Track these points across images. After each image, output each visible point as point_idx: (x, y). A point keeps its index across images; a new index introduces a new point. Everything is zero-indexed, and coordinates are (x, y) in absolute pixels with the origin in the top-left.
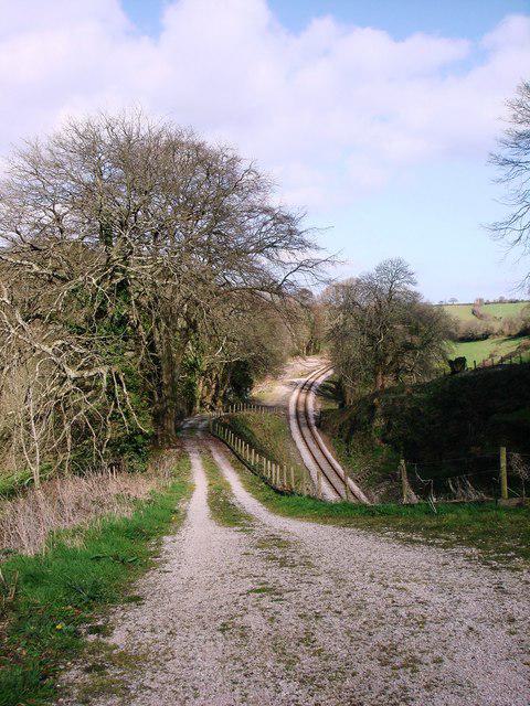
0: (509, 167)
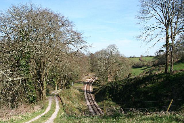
0: (142, 19)
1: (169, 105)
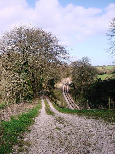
0: (111, 37)
1: (108, 102)
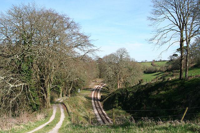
0: (154, 21)
1: (184, 113)
